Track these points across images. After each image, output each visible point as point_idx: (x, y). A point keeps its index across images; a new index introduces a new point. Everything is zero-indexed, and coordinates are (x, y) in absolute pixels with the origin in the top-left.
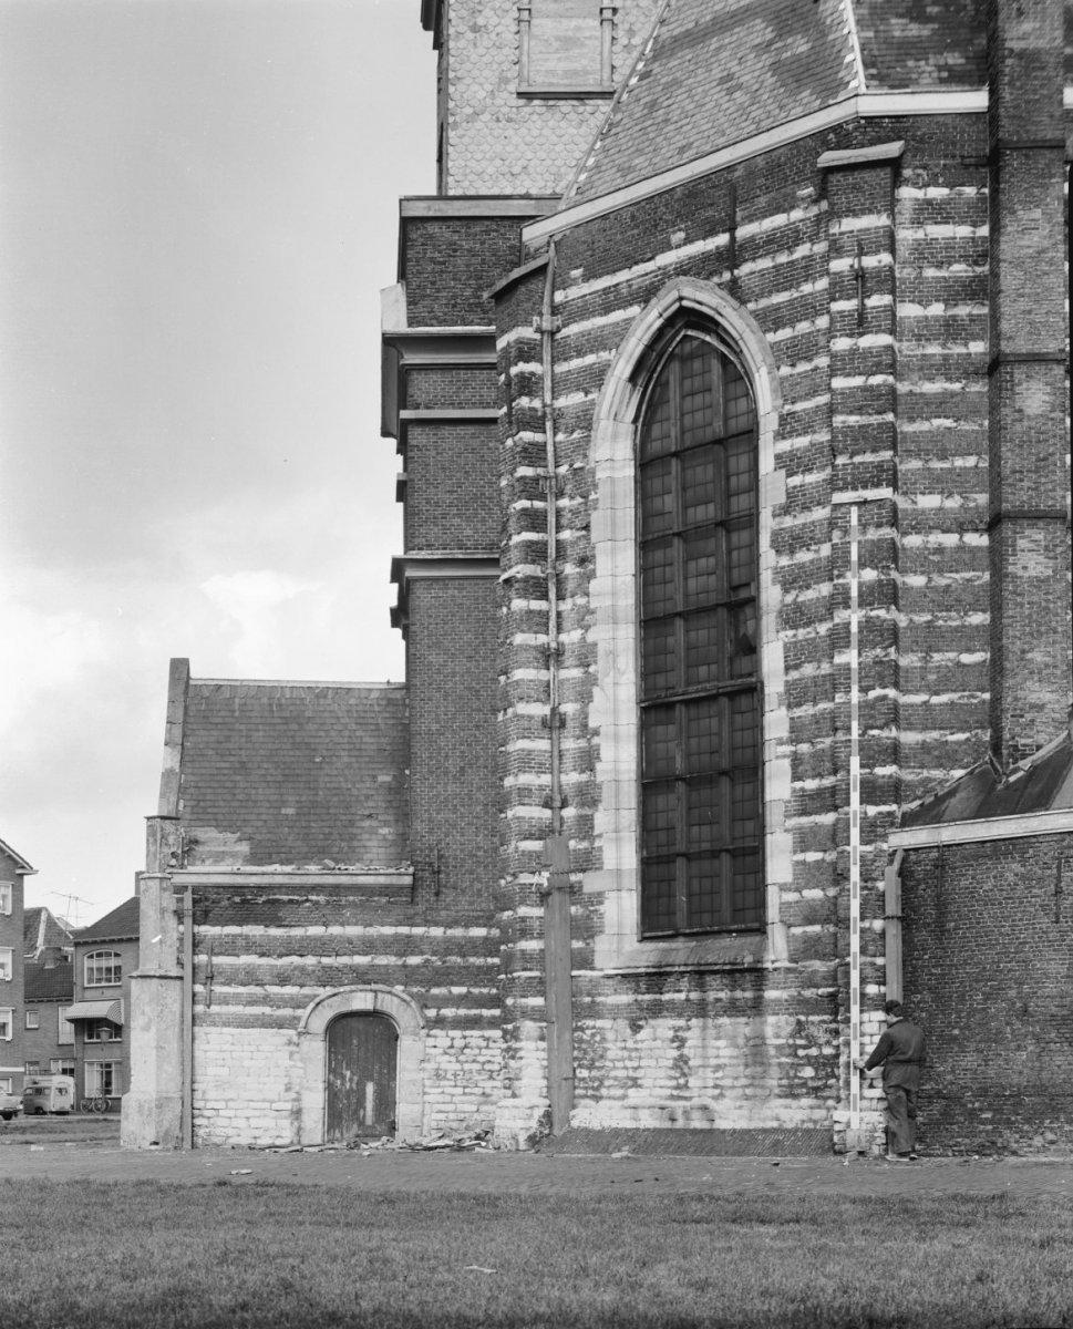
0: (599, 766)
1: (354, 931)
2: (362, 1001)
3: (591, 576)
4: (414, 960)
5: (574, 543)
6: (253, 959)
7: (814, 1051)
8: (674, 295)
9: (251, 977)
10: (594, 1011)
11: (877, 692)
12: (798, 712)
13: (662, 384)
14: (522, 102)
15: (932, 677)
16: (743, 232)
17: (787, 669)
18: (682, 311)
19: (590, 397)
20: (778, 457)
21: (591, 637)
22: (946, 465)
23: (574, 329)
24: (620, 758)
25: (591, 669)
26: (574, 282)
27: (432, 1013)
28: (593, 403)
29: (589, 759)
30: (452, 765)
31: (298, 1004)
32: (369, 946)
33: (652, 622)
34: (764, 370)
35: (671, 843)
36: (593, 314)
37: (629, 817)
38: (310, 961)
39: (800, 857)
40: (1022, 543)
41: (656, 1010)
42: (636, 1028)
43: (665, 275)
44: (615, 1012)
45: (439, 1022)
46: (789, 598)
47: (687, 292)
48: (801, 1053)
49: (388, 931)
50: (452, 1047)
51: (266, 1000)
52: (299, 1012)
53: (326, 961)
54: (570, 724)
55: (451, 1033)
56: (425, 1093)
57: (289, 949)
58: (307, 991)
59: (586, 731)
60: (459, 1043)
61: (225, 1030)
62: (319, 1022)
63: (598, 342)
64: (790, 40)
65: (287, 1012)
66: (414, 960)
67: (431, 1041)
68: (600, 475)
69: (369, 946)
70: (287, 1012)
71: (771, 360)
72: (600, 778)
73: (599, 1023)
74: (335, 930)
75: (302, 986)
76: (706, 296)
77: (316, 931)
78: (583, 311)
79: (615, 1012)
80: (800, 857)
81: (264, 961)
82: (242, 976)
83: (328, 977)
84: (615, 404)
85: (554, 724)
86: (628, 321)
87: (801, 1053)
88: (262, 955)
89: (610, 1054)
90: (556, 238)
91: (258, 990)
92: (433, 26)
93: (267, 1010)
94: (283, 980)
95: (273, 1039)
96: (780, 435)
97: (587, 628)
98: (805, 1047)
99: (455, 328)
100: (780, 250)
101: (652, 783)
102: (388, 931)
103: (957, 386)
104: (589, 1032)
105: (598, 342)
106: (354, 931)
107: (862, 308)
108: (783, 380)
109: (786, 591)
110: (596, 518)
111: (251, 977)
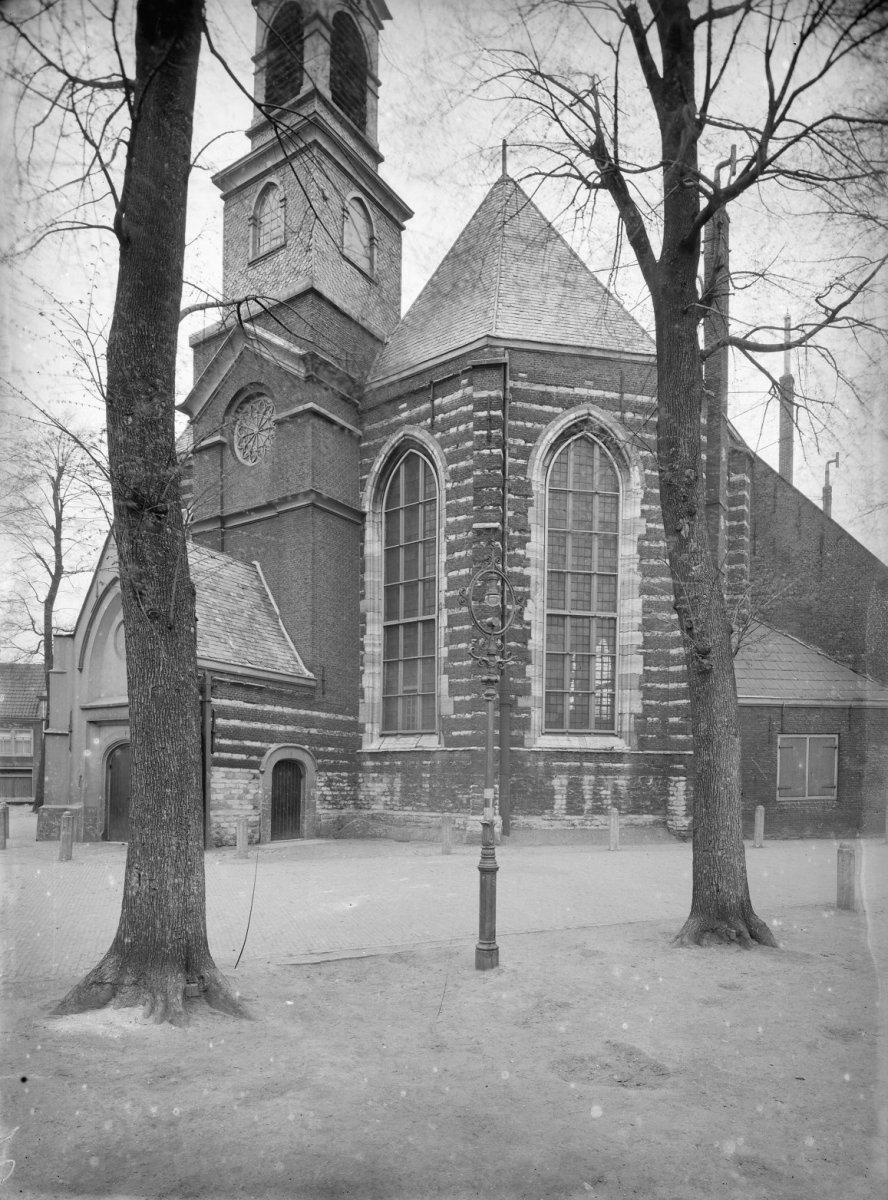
0: (530, 642)
16: (628, 396)
20: (643, 511)
28: (531, 448)
47: (593, 412)
62: (268, 763)
66: (313, 731)
72: (529, 647)
86: (557, 414)
108: (646, 475)
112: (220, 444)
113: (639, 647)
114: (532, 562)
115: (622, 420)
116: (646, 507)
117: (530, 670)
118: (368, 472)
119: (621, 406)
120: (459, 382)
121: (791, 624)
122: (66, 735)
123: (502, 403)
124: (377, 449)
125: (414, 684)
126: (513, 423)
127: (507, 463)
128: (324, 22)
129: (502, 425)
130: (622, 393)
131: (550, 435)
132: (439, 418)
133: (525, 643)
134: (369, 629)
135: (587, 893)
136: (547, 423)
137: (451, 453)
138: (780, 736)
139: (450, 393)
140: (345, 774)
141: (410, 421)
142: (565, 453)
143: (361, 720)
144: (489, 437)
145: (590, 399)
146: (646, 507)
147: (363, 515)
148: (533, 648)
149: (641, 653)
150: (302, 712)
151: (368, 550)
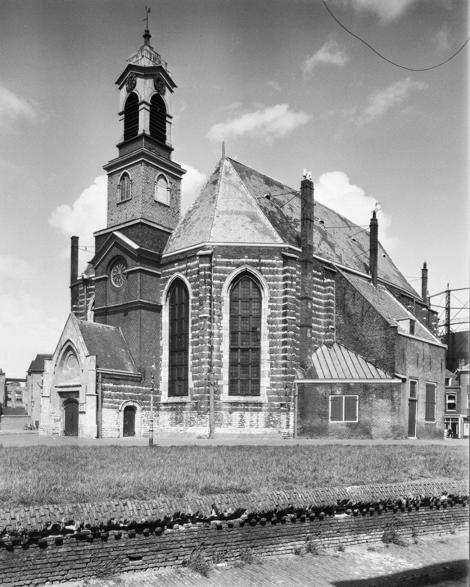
0: (222, 359)
1: (130, 387)
2: (131, 404)
3: (221, 319)
4: (140, 394)
5: (217, 312)
8: (245, 268)
10: (220, 409)
11: (293, 354)
12: (272, 355)
16: (262, 261)
17: (270, 346)
18: (246, 271)
19: (222, 282)
20: (269, 306)
21: (221, 332)
23: (218, 267)
25: (221, 338)
27: (143, 407)
28: (223, 284)
30: (147, 350)
33: (233, 333)
36: (224, 265)
37: (227, 370)
39: (272, 382)
41: (236, 410)
42: (231, 413)
44: (225, 410)
46: (271, 333)
47: (248, 268)
51: (113, 402)
59: (219, 350)
60: (147, 414)
66: (140, 394)
67: (143, 413)
70: (117, 405)
72: (222, 362)
73: (221, 412)
76: (254, 271)
78: (221, 264)
79: (225, 410)
83: (124, 397)
88: (112, 391)
89: (224, 418)
90: (214, 247)
93: (113, 404)
94: (116, 397)
95: (114, 412)
97: (220, 330)
99: (290, 254)
100: (271, 266)
101: (233, 364)
105: (225, 272)
106: (130, 387)
107: (292, 283)
108: (271, 291)
112: (105, 279)
113: (268, 360)
115: (260, 271)
116: (271, 304)
117: (222, 370)
118: (163, 289)
120: (196, 258)
121: (351, 345)
122: (49, 397)
123: (210, 269)
124: (167, 280)
126: (215, 274)
128: (147, 104)
129: (210, 276)
131: (230, 278)
132: (189, 271)
133: (220, 359)
134: (164, 352)
136: (229, 274)
137: (193, 285)
138: (330, 396)
139: (193, 261)
141: (180, 271)
142: (238, 284)
143: (160, 390)
144: (205, 282)
145: (247, 263)
146: (271, 304)
147: (161, 307)
150: (136, 387)
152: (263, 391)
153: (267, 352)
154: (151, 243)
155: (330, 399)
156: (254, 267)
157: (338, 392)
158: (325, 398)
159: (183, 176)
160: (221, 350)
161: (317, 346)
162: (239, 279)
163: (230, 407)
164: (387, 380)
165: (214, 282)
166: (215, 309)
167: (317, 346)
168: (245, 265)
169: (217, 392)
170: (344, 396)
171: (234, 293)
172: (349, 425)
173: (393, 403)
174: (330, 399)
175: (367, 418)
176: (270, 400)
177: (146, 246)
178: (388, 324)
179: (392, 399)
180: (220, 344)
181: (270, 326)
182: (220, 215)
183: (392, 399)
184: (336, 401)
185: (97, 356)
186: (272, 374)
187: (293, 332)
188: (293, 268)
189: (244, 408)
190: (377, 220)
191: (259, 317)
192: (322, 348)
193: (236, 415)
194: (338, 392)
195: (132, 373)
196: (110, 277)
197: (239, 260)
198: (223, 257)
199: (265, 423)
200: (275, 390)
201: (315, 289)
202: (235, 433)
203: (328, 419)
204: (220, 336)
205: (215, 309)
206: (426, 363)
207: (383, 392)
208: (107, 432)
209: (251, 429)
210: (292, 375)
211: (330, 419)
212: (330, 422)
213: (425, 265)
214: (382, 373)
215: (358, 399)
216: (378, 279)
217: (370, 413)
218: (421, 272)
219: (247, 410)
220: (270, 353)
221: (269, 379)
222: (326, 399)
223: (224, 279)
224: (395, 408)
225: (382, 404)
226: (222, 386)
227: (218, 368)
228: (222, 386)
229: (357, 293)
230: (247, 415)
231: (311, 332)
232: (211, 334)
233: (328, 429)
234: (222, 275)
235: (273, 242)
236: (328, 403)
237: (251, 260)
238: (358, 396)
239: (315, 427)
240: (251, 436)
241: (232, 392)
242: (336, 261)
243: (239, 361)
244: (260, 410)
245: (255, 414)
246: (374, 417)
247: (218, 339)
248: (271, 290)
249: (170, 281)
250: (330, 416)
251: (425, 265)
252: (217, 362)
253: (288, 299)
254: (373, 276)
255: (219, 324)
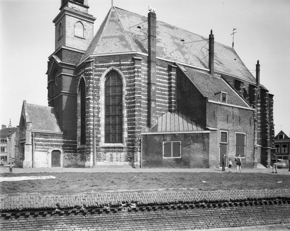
0: (100, 122)
3: (99, 99)
6: (42, 143)
7: (130, 156)
9: (42, 145)
11: (139, 117)
13: (109, 78)
14: (75, 37)
15: (143, 116)
16: (122, 63)
18: (113, 70)
20: (126, 89)
21: (99, 106)
22: (144, 93)
24: (103, 121)
25: (99, 110)
26: (97, 63)
27: (65, 151)
29: (99, 121)
31: (48, 149)
32: (57, 142)
34: (124, 79)
35: (110, 132)
36: (100, 68)
38: (49, 143)
40: (152, 103)
41: (108, 151)
42: (105, 153)
43: (111, 65)
45: (66, 152)
46: (127, 105)
47: (114, 68)
48: (128, 157)
49: (60, 140)
50: (67, 155)
51: (44, 148)
52: (48, 150)
53: (52, 143)
54: (96, 116)
55: (67, 153)
56: (64, 161)
57: (47, 141)
58: (49, 147)
59: (98, 117)
60: (68, 155)
61: (38, 152)
62: (50, 151)
63: (101, 71)
64: (123, 42)
65: (47, 150)
67: (65, 154)
68: (101, 87)
69: (57, 142)
70: (47, 150)
71: (102, 75)
72: (100, 123)
73: (100, 153)
74: (53, 139)
75: (48, 146)
76: (117, 69)
77: (50, 139)
79: (102, 151)
80: (128, 135)
81: (43, 143)
82: (40, 145)
83: (52, 145)
84: (103, 80)
85: (94, 116)
86: (105, 69)
87: (128, 157)
88: (43, 142)
90: (95, 57)
91: (43, 147)
92: (56, 23)
93: (44, 149)
94: (46, 146)
95: (45, 154)
96: (126, 87)
98: (128, 156)
100: (127, 66)
102: (60, 140)
103: (145, 85)
104: (98, 154)
105: (101, 71)
108: (127, 81)
109: (127, 104)
110: (100, 92)
111: (42, 145)
114: (101, 104)
115: (121, 69)
117: (100, 128)
118: (78, 85)
119: (120, 65)
125: (272, 107)
126: (96, 73)
127: (94, 82)
130: (120, 62)
133: (99, 122)
135: (241, 188)
140: (73, 153)
145: (113, 65)
148: (101, 123)
149: (126, 123)
151: (78, 102)
152: (125, 140)
153: (50, 112)
154: (70, 59)
155: (163, 144)
156: (117, 67)
157: (168, 139)
158: (160, 143)
159: (94, 22)
160: (99, 117)
161: (163, 112)
162: (109, 74)
163: (105, 150)
164: (200, 131)
165: (95, 77)
166: (96, 93)
167: (163, 112)
168: (112, 66)
169: (98, 141)
170: (172, 142)
171: (108, 83)
172: (176, 160)
173: (204, 146)
174: (163, 144)
175: (186, 155)
176: (128, 145)
177: (66, 61)
178: (203, 96)
179: (204, 143)
180: (99, 113)
181: (127, 101)
182: (103, 39)
183: (204, 143)
184: (168, 145)
185: (246, 133)
186: (128, 130)
187: (139, 104)
188: (139, 66)
189: (113, 150)
190: (213, 35)
191: (121, 96)
192: (167, 113)
193: (108, 154)
194: (168, 139)
195: (58, 132)
196: (54, 81)
197: (108, 64)
198: (100, 63)
199: (125, 159)
200: (130, 139)
201: (158, 77)
202: (108, 165)
203: (162, 156)
204: (99, 108)
205: (96, 93)
206: (236, 120)
207: (197, 139)
208: (40, 165)
209: (117, 162)
210: (139, 130)
211: (163, 156)
212: (164, 158)
213: (258, 62)
214: (195, 127)
215: (181, 143)
216: (214, 71)
217: (189, 152)
218: (255, 66)
219: (114, 151)
220: (127, 118)
221: (127, 132)
222: (161, 144)
223: (100, 75)
224: (205, 149)
225: (197, 146)
226: (100, 138)
227: (98, 127)
228: (100, 138)
229: (187, 79)
230: (114, 154)
231: (155, 104)
232: (93, 108)
233: (162, 162)
234: (99, 73)
235: (129, 51)
236: (162, 147)
237: (115, 63)
238: (181, 142)
239: (154, 161)
240: (116, 166)
241: (107, 141)
242: (182, 62)
243: (111, 123)
244: (122, 151)
245: (119, 154)
246: (191, 155)
247: (97, 110)
248: (127, 80)
249: (80, 80)
250: (163, 154)
251: (258, 62)
252: (97, 124)
253: (136, 84)
254: (210, 70)
255: (98, 102)
